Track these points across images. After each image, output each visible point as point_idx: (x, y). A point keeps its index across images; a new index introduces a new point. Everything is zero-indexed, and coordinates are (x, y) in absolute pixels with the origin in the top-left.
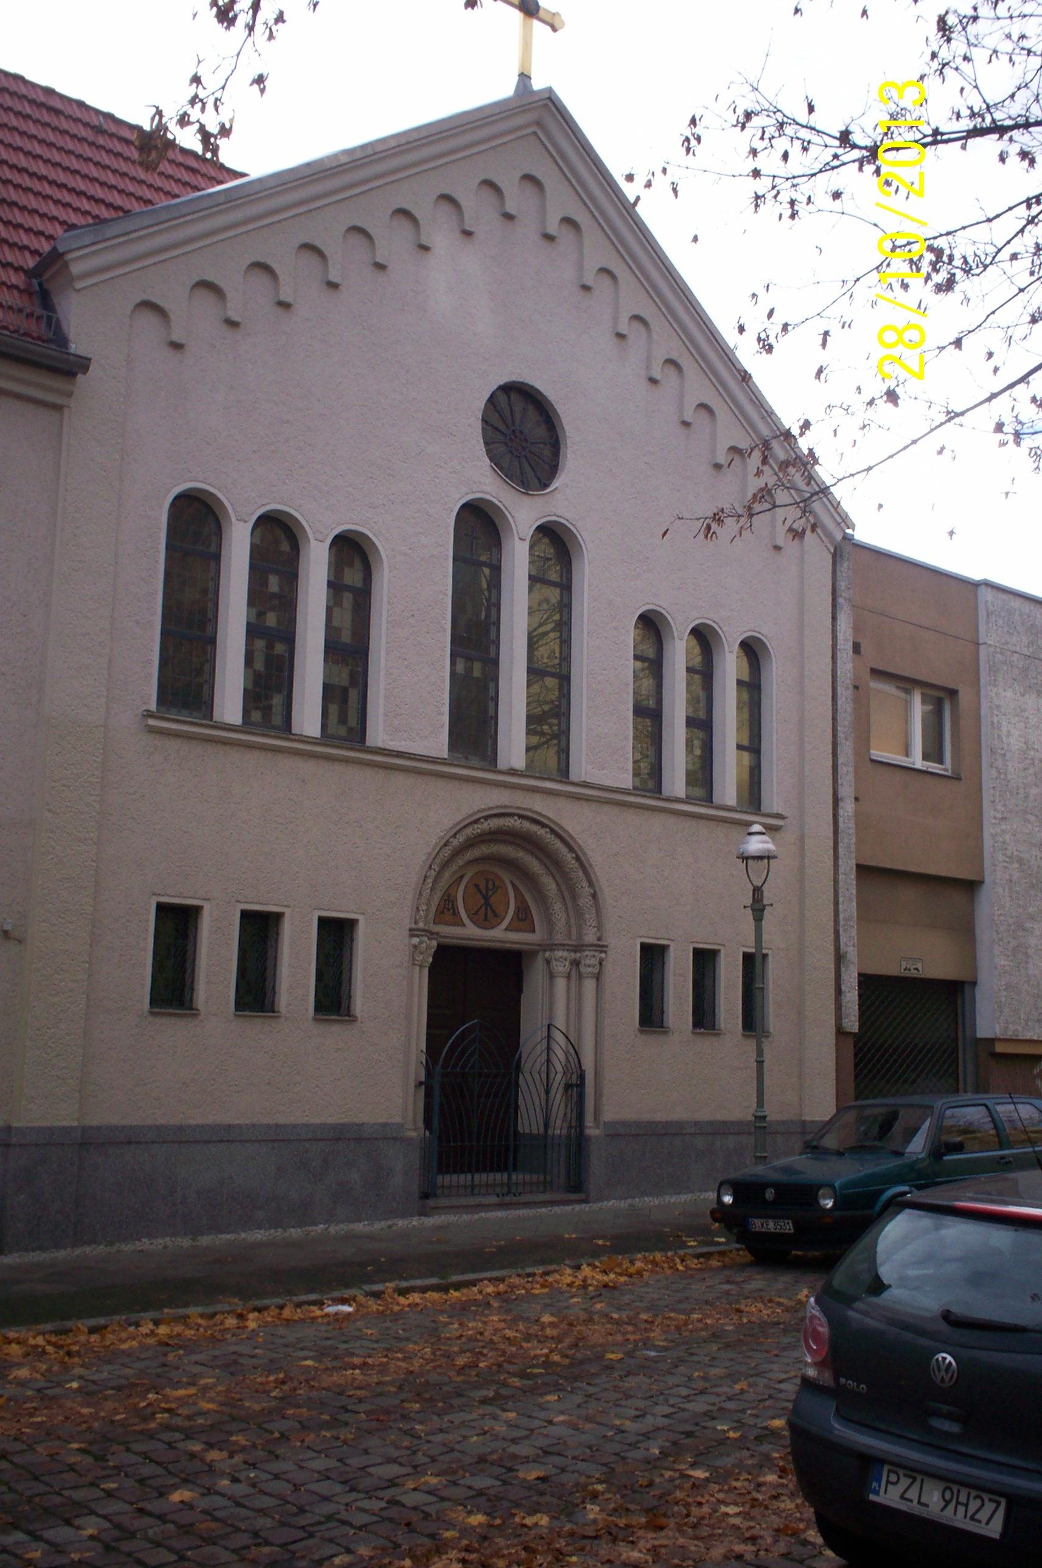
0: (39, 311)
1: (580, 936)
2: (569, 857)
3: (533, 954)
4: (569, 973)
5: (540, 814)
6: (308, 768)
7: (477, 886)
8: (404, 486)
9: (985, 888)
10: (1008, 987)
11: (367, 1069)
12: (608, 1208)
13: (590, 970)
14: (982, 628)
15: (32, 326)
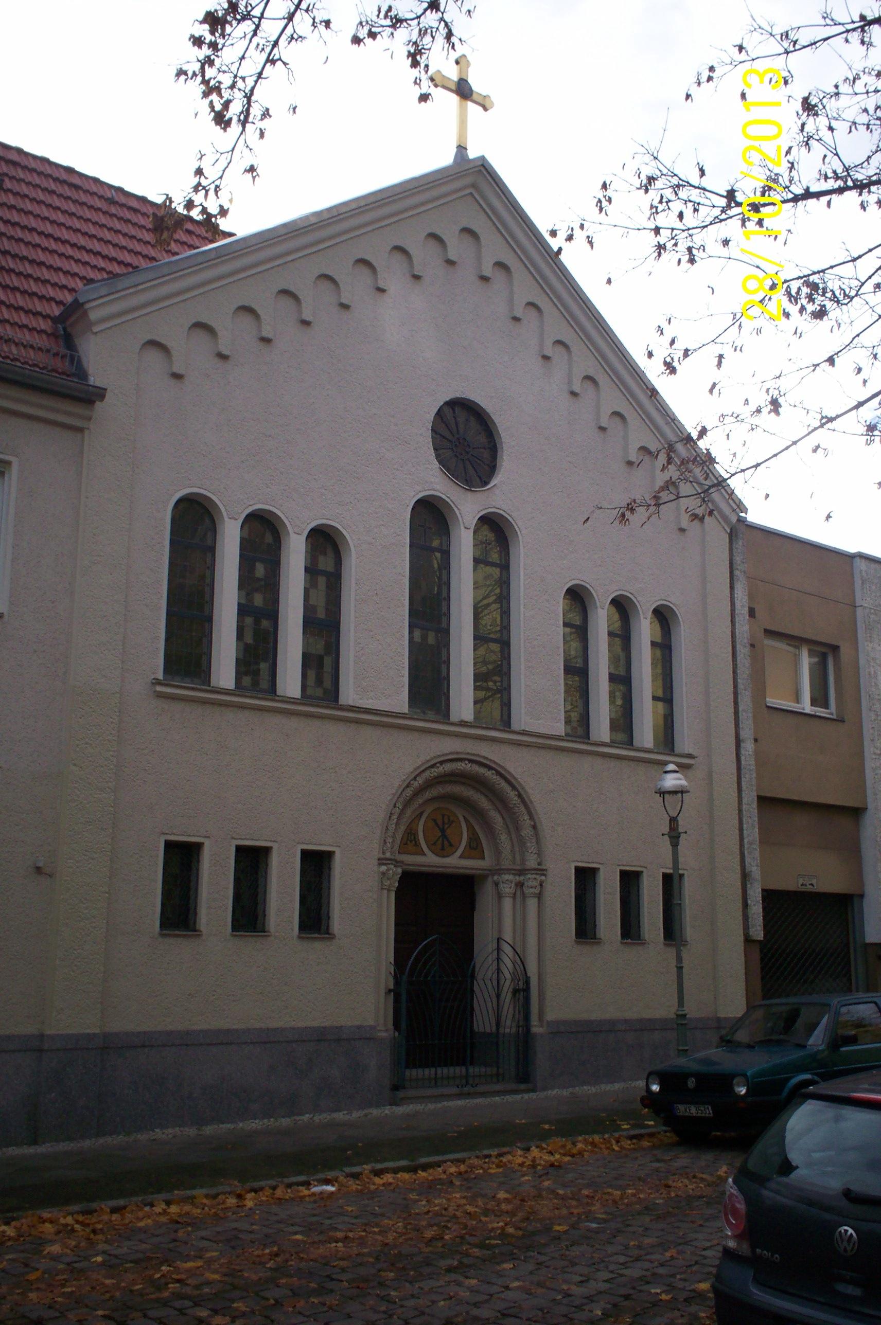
0: (63, 351)
1: (523, 861)
3: (484, 878)
4: (515, 894)
5: (486, 758)
6: (293, 723)
7: (435, 820)
8: (364, 485)
11: (342, 981)
13: (532, 890)
15: (59, 364)
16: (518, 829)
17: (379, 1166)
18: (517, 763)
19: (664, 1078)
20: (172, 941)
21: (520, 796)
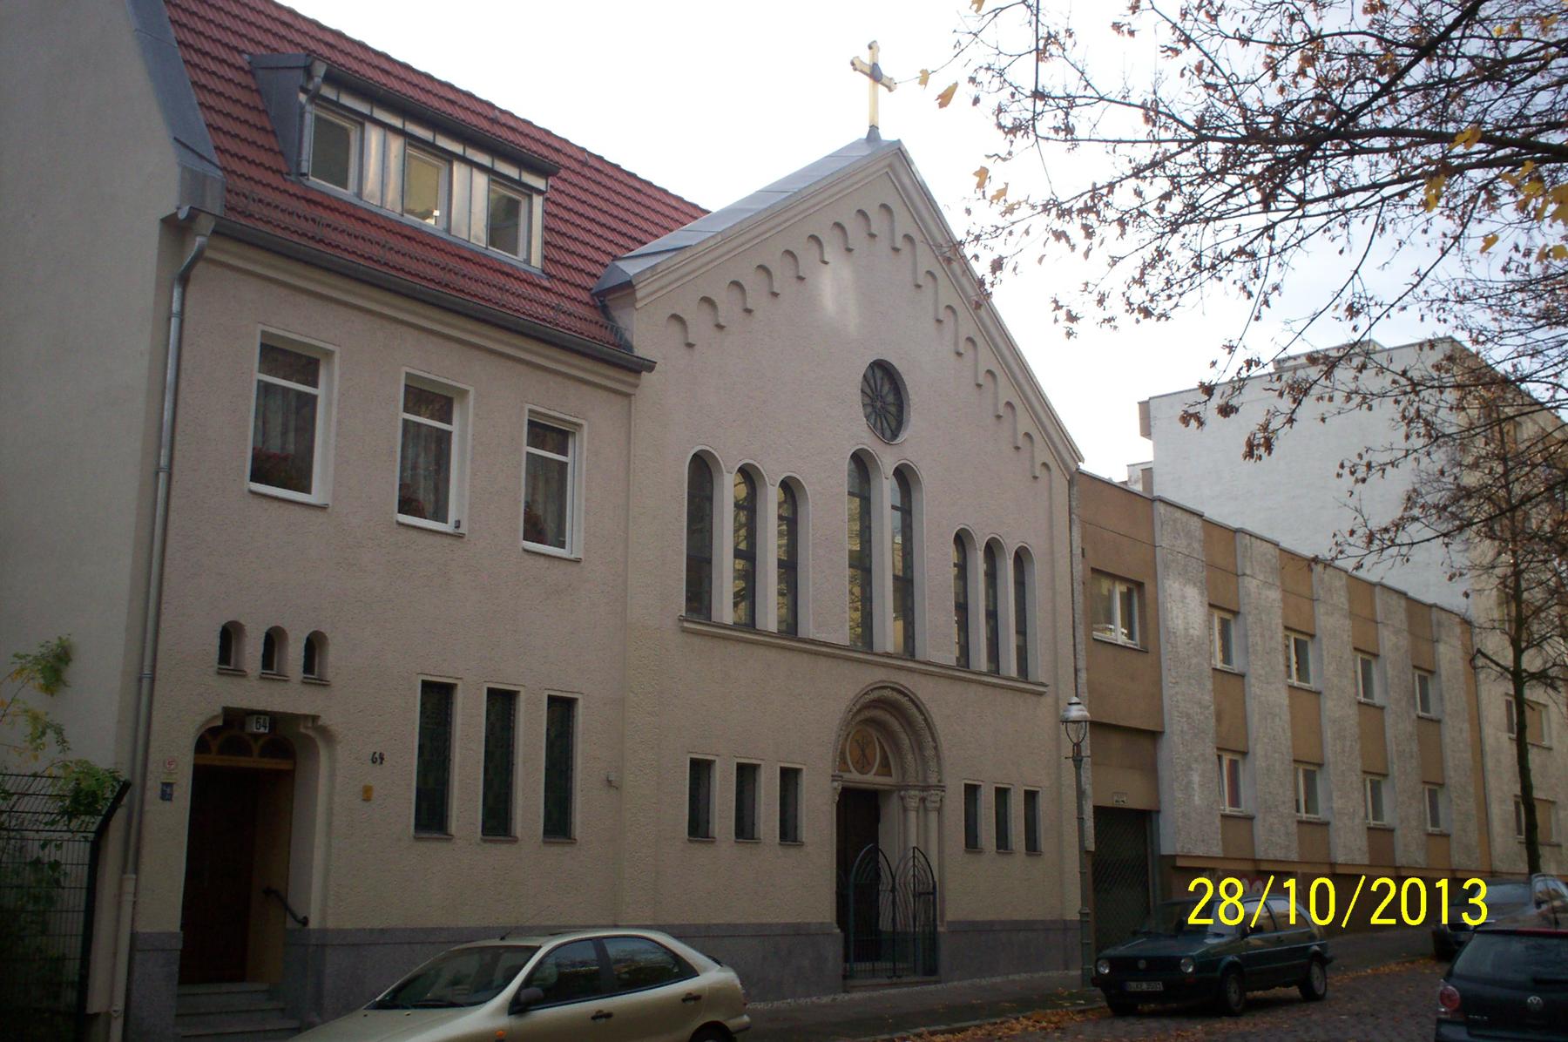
0: (602, 320)
1: (925, 779)
2: (920, 718)
3: (887, 793)
6: (772, 655)
8: (815, 439)
9: (1166, 737)
10: (1184, 814)
11: (796, 884)
12: (953, 988)
14: (1158, 534)
15: (595, 330)
16: (921, 748)
17: (932, 1029)
18: (924, 689)
19: (1114, 963)
20: (696, 845)
21: (926, 720)
